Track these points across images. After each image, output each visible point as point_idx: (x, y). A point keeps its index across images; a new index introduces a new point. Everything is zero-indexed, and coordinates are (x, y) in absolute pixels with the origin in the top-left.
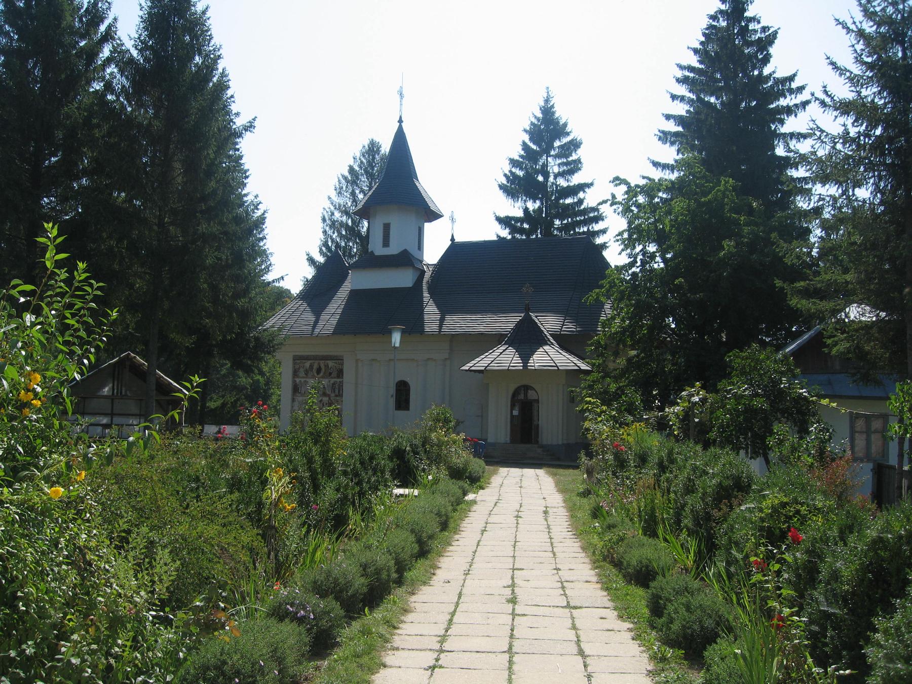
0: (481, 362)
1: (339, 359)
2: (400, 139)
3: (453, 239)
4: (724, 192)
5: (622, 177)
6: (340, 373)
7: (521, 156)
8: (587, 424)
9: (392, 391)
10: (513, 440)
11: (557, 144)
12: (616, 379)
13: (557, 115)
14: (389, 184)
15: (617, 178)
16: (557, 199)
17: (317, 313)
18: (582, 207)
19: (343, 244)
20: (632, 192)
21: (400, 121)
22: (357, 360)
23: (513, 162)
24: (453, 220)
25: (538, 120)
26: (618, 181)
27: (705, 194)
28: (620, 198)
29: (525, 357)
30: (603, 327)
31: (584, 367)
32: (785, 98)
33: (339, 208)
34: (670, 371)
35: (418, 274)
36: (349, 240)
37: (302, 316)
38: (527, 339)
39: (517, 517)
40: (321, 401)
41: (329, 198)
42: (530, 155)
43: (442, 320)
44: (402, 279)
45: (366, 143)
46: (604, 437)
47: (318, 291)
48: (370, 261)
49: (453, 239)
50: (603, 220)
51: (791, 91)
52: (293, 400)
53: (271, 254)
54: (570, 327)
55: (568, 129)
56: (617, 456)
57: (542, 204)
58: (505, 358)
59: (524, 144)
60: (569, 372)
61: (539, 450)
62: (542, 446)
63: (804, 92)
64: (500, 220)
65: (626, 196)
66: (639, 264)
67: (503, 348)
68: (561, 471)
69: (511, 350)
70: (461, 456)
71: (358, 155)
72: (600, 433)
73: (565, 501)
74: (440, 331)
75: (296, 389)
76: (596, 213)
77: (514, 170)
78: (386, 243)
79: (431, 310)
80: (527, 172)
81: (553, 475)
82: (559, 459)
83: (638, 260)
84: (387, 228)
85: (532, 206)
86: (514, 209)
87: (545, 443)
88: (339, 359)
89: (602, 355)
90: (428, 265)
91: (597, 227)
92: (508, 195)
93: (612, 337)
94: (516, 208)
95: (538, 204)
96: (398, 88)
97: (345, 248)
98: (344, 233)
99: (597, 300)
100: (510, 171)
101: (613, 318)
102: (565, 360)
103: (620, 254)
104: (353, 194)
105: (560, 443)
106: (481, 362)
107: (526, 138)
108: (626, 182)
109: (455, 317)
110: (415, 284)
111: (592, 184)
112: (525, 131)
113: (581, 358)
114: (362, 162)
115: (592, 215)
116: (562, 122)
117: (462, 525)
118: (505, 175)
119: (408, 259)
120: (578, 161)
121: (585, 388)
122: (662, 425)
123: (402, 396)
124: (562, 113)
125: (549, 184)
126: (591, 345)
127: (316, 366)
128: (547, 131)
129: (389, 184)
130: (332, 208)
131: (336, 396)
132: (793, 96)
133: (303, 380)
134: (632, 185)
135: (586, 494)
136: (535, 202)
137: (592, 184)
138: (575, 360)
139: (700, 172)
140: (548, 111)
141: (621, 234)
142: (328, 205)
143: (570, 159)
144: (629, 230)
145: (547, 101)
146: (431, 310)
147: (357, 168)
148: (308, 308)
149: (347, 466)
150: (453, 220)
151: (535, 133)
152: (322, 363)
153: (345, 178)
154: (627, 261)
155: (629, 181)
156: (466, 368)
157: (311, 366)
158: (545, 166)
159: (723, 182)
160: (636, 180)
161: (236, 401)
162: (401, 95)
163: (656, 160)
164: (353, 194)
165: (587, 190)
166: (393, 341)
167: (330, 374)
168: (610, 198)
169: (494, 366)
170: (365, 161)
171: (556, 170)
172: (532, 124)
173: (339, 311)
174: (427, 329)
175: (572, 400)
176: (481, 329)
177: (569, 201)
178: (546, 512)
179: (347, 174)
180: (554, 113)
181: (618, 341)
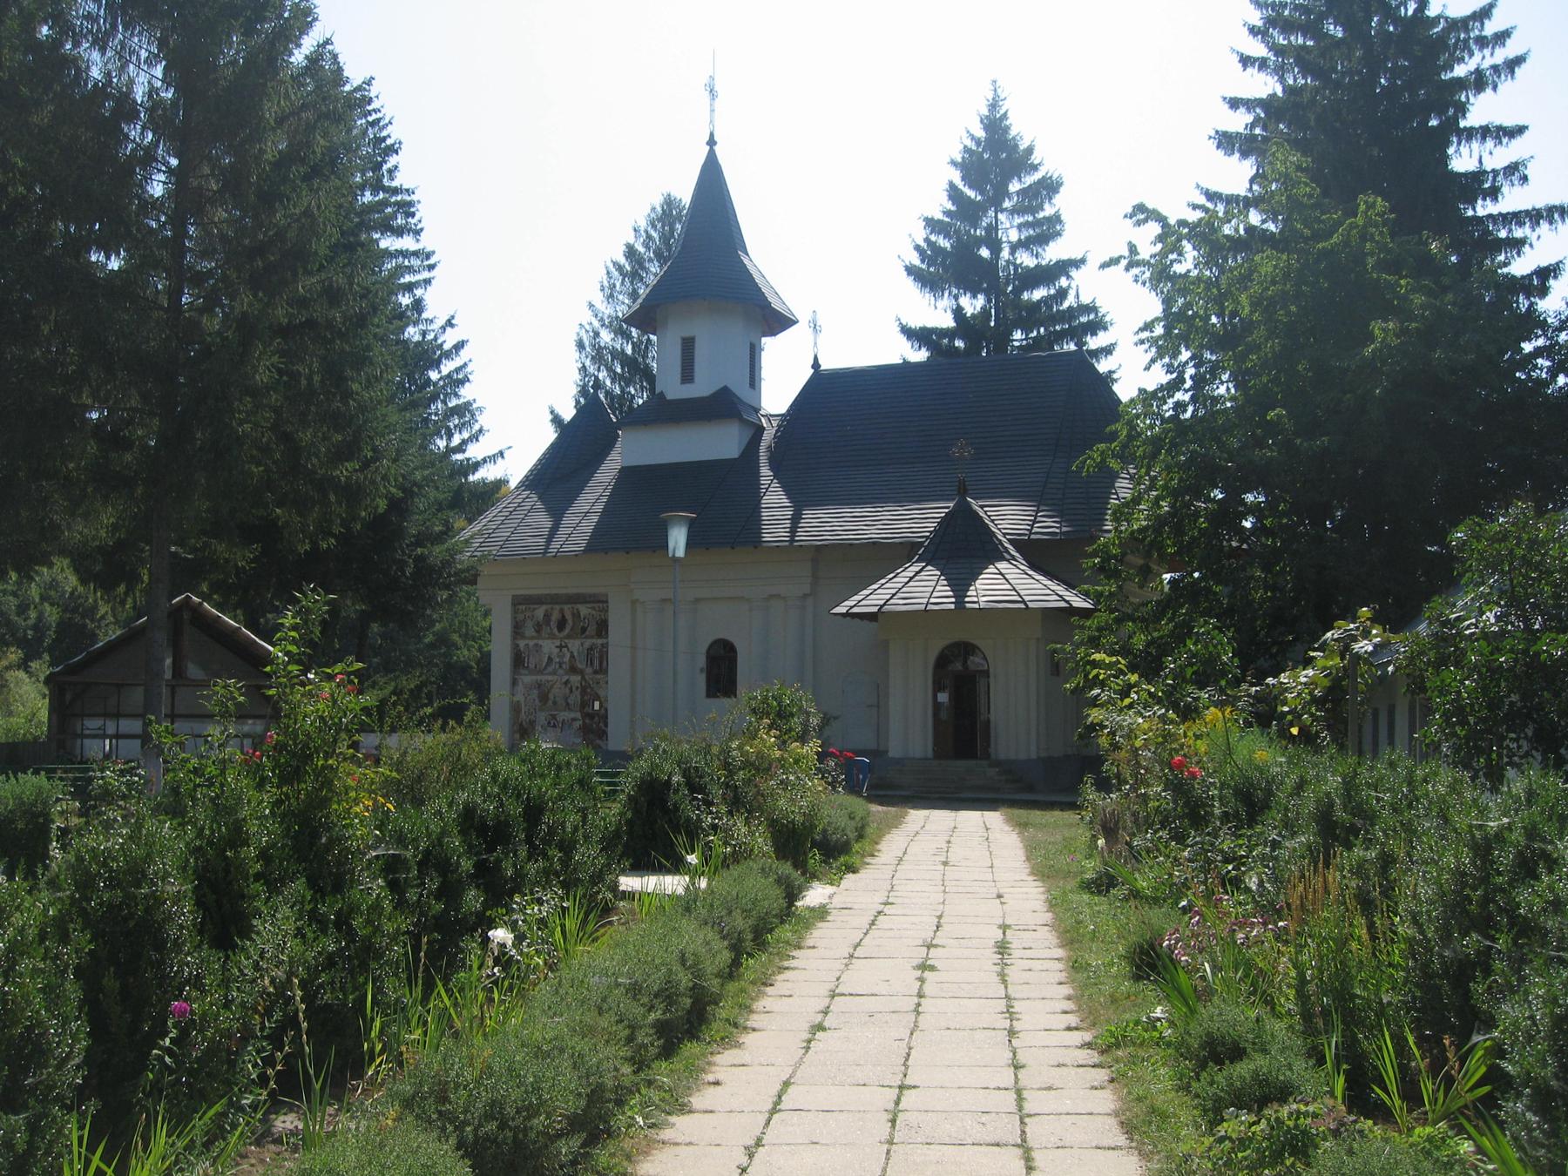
0: (870, 599)
1: (600, 601)
2: (711, 179)
3: (816, 365)
4: (1365, 227)
5: (1150, 206)
6: (602, 628)
7: (947, 213)
8: (1095, 715)
9: (702, 661)
10: (938, 754)
11: (1014, 186)
12: (1147, 623)
13: (1013, 133)
14: (696, 271)
15: (1140, 208)
16: (1018, 291)
17: (557, 514)
18: (1066, 305)
19: (618, 391)
20: (1171, 237)
21: (712, 142)
22: (634, 602)
23: (931, 224)
24: (815, 328)
25: (978, 142)
26: (1141, 213)
27: (1317, 237)
28: (1147, 250)
29: (960, 586)
30: (1116, 520)
31: (1079, 602)
32: (1471, 55)
34: (1263, 600)
35: (748, 434)
36: (628, 382)
37: (528, 519)
38: (962, 549)
39: (924, 967)
40: (567, 683)
41: (591, 306)
42: (964, 210)
43: (796, 519)
45: (658, 201)
46: (1138, 743)
47: (559, 474)
48: (664, 413)
49: (816, 365)
50: (1105, 329)
51: (1482, 42)
52: (514, 683)
53: (480, 409)
54: (1048, 526)
56: (1179, 788)
57: (989, 301)
58: (921, 588)
59: (952, 186)
60: (1049, 614)
62: (998, 763)
63: (1508, 42)
64: (909, 333)
65: (1160, 246)
66: (1189, 384)
67: (915, 568)
68: (1037, 815)
69: (932, 572)
70: (810, 794)
72: (1131, 734)
73: (1052, 905)
74: (792, 541)
75: (518, 661)
76: (1092, 316)
77: (933, 238)
78: (687, 375)
79: (775, 501)
80: (959, 240)
81: (1022, 826)
82: (1031, 788)
83: (1187, 376)
84: (688, 345)
85: (972, 305)
86: (937, 314)
87: (1002, 756)
88: (600, 601)
89: (1115, 574)
90: (769, 417)
91: (1093, 343)
92: (924, 285)
93: (1135, 539)
94: (940, 311)
95: (980, 301)
96: (706, 80)
97: (621, 397)
98: (619, 370)
99: (1102, 466)
100: (927, 240)
101: (1136, 500)
103: (1147, 368)
105: (1034, 756)
106: (870, 599)
108: (1162, 219)
109: (820, 513)
110: (743, 455)
111: (1083, 261)
112: (953, 163)
113: (1070, 585)
114: (649, 237)
115: (1084, 319)
116: (1023, 146)
117: (758, 1005)
118: (917, 248)
119: (730, 406)
120: (1056, 219)
121: (1082, 643)
122: (1265, 715)
123: (721, 670)
124: (1022, 128)
125: (1002, 263)
126: (1094, 554)
127: (555, 616)
128: (995, 163)
129: (696, 271)
130: (596, 324)
131: (596, 672)
132: (1487, 52)
133: (531, 643)
134: (1172, 221)
135: (1102, 885)
136: (974, 296)
137: (1083, 261)
138: (1061, 590)
139: (1310, 196)
140: (995, 126)
141: (1148, 326)
142: (587, 317)
143: (1041, 215)
144: (1170, 318)
145: (993, 106)
146: (775, 501)
147: (641, 249)
148: (539, 505)
149: (401, 840)
150: (815, 328)
152: (567, 608)
153: (620, 268)
154: (1165, 378)
155: (1164, 213)
156: (841, 609)
157: (547, 616)
158: (993, 229)
159: (1362, 207)
160: (1179, 209)
161: (419, 688)
163: (1214, 188)
165: (1074, 273)
166: (671, 545)
167: (584, 630)
168: (1127, 254)
169: (898, 605)
170: (655, 234)
171: (1014, 236)
172: (966, 150)
173: (599, 507)
174: (767, 538)
175: (1056, 669)
176: (873, 533)
177: (1039, 294)
178: (1002, 948)
179: (622, 261)
180: (1007, 128)
181: (1149, 547)
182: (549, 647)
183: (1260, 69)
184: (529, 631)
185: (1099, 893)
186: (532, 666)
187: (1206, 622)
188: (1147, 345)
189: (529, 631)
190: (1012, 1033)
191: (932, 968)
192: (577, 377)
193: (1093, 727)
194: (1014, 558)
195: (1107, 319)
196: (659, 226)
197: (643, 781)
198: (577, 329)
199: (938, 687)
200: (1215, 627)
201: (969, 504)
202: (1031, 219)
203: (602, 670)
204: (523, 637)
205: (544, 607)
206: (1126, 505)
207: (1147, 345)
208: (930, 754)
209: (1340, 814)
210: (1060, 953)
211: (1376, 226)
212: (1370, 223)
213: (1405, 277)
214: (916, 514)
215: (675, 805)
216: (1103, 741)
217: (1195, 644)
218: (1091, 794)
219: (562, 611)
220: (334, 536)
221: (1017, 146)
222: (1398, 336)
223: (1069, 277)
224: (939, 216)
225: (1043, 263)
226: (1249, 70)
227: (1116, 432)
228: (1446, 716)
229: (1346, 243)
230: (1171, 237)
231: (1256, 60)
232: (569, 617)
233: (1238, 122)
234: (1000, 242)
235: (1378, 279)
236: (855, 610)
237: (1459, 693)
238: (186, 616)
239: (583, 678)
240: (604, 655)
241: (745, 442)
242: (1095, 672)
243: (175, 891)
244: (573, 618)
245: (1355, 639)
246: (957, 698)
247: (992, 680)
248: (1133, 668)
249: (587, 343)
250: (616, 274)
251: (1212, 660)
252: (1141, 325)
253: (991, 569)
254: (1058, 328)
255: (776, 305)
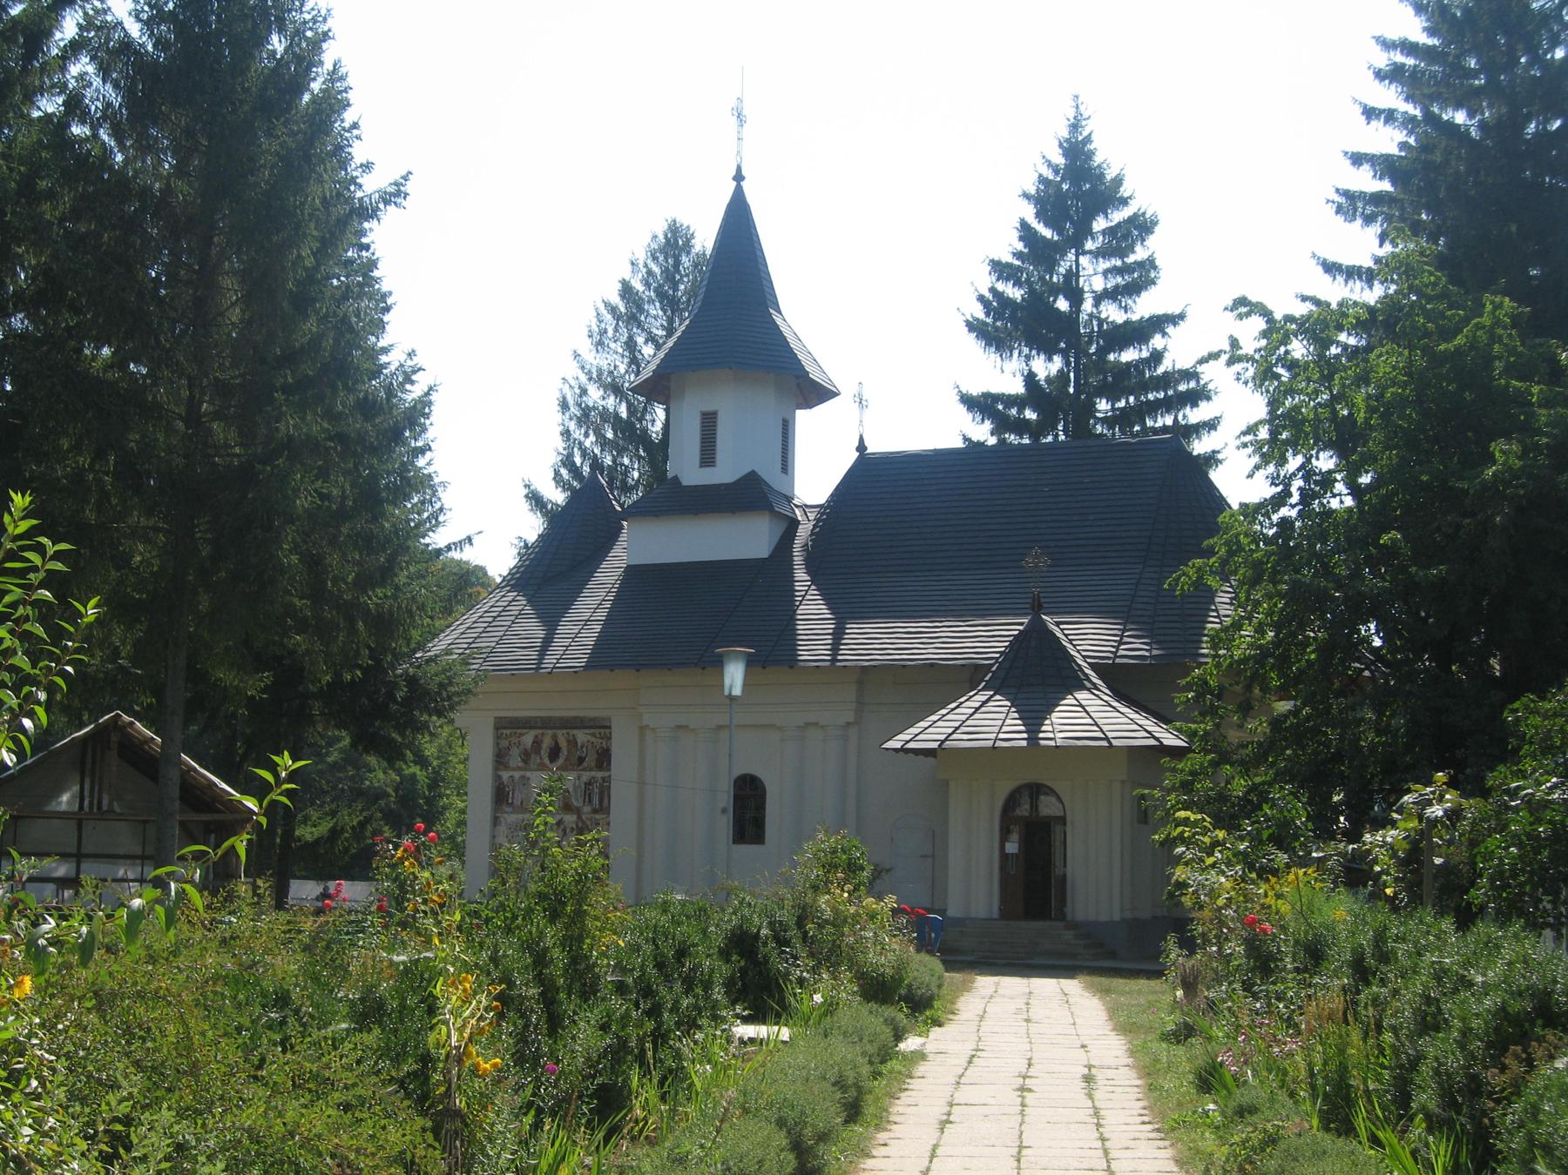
0: (930, 731)
1: (601, 726)
2: (738, 219)
3: (861, 447)
4: (1493, 326)
5: (1253, 298)
6: (604, 758)
10: (1006, 914)
11: (1099, 224)
12: (1246, 767)
13: (1098, 159)
14: (716, 320)
15: (1241, 302)
16: (1103, 352)
18: (1160, 370)
19: (608, 461)
20: (1277, 332)
21: (739, 177)
22: (642, 729)
23: (1000, 269)
24: (861, 402)
26: (1244, 306)
29: (1033, 719)
30: (1215, 647)
31: (1170, 740)
33: (598, 378)
35: (780, 528)
36: (621, 452)
37: (516, 627)
38: (1036, 676)
41: (576, 355)
42: (1038, 252)
43: (838, 635)
44: (744, 540)
45: (660, 229)
46: (1221, 902)
47: (551, 570)
48: (671, 499)
49: (861, 447)
50: (1209, 398)
52: (496, 821)
54: (1136, 648)
55: (1125, 191)
57: (1068, 364)
58: (987, 720)
59: (1024, 226)
61: (1068, 935)
62: (1075, 926)
65: (1264, 342)
66: (1295, 498)
67: (981, 698)
68: (1118, 983)
69: (1000, 704)
71: (641, 256)
72: (1213, 893)
73: (1132, 1053)
75: (501, 796)
76: (1192, 384)
77: (1000, 286)
78: (708, 457)
81: (1104, 992)
82: (1113, 955)
84: (709, 422)
85: (1046, 368)
86: (1004, 375)
88: (601, 726)
89: (1212, 711)
90: (804, 507)
91: (1194, 415)
92: (988, 344)
93: (1235, 668)
94: (1008, 375)
96: (734, 103)
98: (610, 435)
99: (1199, 584)
100: (993, 290)
101: (1237, 626)
102: (1124, 725)
103: (1250, 476)
104: (631, 345)
105: (1117, 917)
106: (930, 731)
107: (1029, 212)
108: (1266, 313)
109: (868, 627)
111: (1182, 316)
113: (1163, 718)
114: (650, 273)
115: (1182, 387)
116: (1110, 175)
117: (893, 1110)
118: (981, 299)
119: (756, 495)
120: (1150, 264)
122: (1356, 874)
123: (748, 810)
124: (1109, 155)
125: (1083, 317)
126: (1188, 687)
127: (547, 742)
128: (1077, 197)
129: (716, 320)
130: (583, 378)
131: (595, 811)
133: (517, 774)
134: (1278, 316)
135: (1184, 1033)
136: (1050, 359)
138: (1149, 724)
139: (1435, 284)
140: (1077, 152)
142: (572, 371)
143: (1131, 259)
145: (1075, 127)
146: (813, 611)
150: (861, 402)
151: (1049, 202)
152: (562, 736)
153: (613, 310)
154: (1269, 491)
155: (1270, 307)
156: (894, 744)
157: (537, 743)
158: (1073, 275)
159: (1489, 307)
160: (1286, 306)
161: (362, 825)
162: (740, 118)
163: (1332, 258)
164: (631, 345)
165: (1170, 330)
166: (727, 681)
167: (581, 760)
168: (1228, 348)
169: (962, 741)
170: (656, 269)
171: (1099, 284)
172: (1042, 180)
173: (602, 614)
174: (804, 656)
175: (1143, 817)
176: (930, 653)
177: (1129, 355)
179: (616, 300)
181: (1249, 679)
182: (538, 779)
183: (1386, 122)
184: (515, 760)
185: (1179, 1042)
186: (517, 802)
187: (1282, 788)
188: (1250, 449)
189: (515, 760)
190: (1098, 1125)
191: (1030, 1090)
192: (560, 444)
193: (1182, 885)
194: (1096, 687)
195: (1210, 387)
196: (661, 258)
197: (733, 934)
198: (560, 384)
199: (1005, 833)
200: (1291, 793)
201: (1043, 623)
202: (1119, 263)
203: (603, 809)
204: (507, 767)
205: (533, 733)
206: (1225, 629)
207: (1250, 449)
208: (996, 914)
209: (1370, 962)
210: (1139, 1082)
211: (1505, 328)
212: (1497, 323)
213: (1538, 383)
214: (981, 631)
215: (764, 957)
216: (1187, 901)
217: (1271, 808)
218: (1174, 953)
219: (554, 737)
220: (360, 667)
221: (1102, 175)
222: (1519, 458)
223: (1164, 334)
224: (1007, 258)
225: (1135, 317)
226: (1374, 123)
227: (1213, 547)
228: (1492, 880)
229: (1473, 344)
230: (1277, 332)
231: (1382, 111)
232: (563, 744)
233: (1367, 182)
234: (1081, 291)
235: (1507, 386)
236: (911, 745)
237: (1501, 859)
238: (114, 738)
239: (579, 817)
240: (605, 791)
241: (776, 539)
242: (1180, 829)
243: (652, 971)
244: (567, 750)
245: (1429, 803)
246: (1026, 843)
247: (1069, 829)
248: (1217, 825)
249: (571, 402)
250: (608, 317)
251: (1286, 824)
252: (1244, 428)
253: (1069, 700)
254: (1151, 397)
255: (815, 375)
